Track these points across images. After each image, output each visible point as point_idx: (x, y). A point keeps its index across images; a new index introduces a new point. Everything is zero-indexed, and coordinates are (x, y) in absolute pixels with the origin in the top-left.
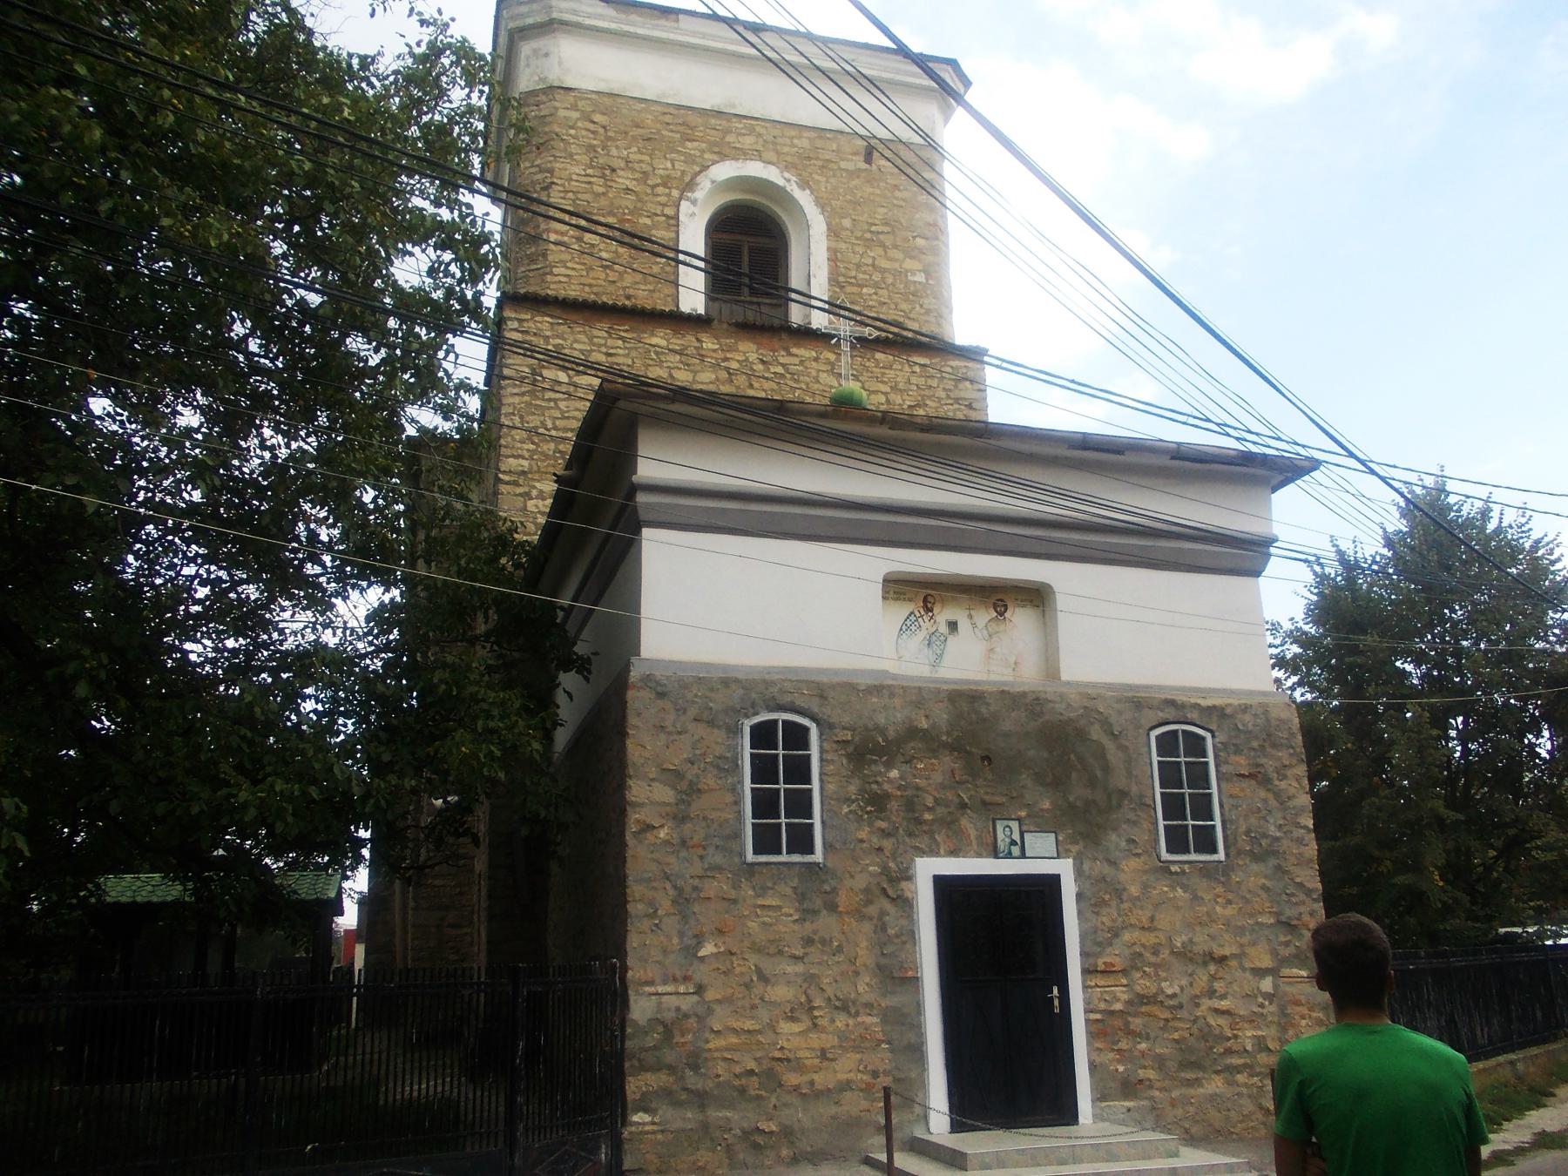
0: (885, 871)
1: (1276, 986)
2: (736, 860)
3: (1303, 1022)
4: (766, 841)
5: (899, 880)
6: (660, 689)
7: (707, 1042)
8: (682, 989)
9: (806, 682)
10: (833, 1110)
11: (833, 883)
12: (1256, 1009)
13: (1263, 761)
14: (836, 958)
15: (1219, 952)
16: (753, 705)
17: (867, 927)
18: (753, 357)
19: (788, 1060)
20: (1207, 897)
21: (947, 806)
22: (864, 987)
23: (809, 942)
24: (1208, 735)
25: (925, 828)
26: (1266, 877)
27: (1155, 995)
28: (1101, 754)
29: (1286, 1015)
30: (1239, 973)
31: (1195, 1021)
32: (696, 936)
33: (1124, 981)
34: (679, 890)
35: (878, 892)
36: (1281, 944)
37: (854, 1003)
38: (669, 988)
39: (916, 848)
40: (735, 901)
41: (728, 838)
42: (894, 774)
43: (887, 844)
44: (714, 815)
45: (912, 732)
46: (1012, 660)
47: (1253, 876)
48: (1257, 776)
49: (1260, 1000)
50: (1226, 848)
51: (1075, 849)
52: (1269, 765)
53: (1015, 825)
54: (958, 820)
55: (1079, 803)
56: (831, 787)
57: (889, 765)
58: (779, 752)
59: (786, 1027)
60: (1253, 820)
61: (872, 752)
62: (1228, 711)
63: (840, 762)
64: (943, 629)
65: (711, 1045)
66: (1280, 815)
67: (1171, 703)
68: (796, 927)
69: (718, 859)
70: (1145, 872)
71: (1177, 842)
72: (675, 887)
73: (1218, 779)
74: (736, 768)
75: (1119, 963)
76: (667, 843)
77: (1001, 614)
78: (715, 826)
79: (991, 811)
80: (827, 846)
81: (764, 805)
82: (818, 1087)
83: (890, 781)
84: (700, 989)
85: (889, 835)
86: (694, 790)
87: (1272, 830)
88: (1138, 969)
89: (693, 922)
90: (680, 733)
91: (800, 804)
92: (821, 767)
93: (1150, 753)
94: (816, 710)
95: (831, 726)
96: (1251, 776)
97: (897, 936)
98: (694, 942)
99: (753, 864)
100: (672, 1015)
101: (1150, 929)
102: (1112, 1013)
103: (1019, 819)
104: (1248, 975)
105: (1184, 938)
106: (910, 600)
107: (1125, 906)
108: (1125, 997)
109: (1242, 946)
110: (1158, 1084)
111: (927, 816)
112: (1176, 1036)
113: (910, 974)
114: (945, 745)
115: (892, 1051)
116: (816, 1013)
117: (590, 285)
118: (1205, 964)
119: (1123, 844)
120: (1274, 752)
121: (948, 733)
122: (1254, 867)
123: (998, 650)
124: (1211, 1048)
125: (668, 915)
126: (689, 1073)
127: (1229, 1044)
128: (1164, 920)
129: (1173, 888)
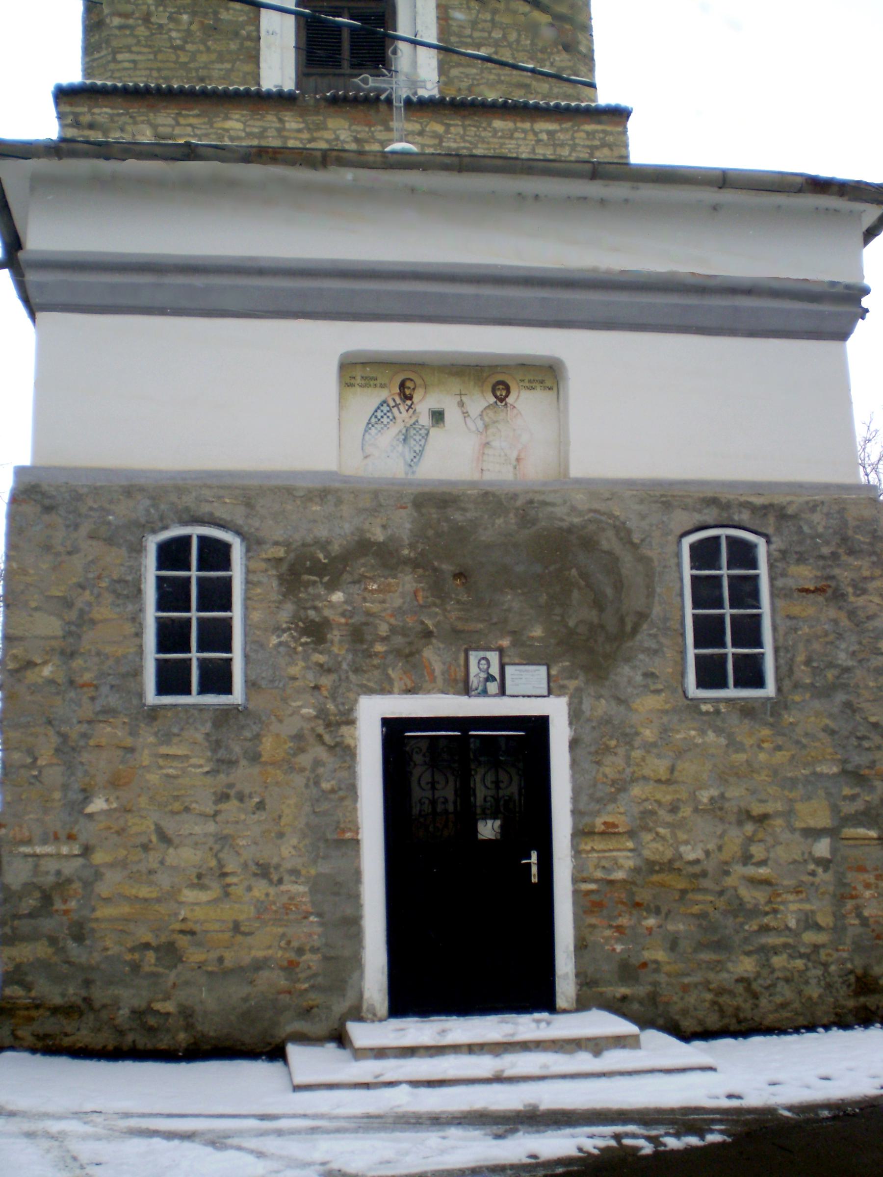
0: (322, 713)
1: (834, 850)
2: (135, 702)
3: (868, 894)
4: (172, 680)
5: (339, 724)
6: (47, 502)
7: (94, 910)
8: (65, 850)
9: (229, 487)
10: (246, 990)
11: (256, 728)
12: (807, 878)
13: (836, 571)
14: (256, 817)
15: (757, 809)
16: (162, 518)
17: (299, 780)
18: (344, 135)
19: (192, 933)
20: (748, 742)
21: (404, 635)
22: (288, 852)
23: (223, 797)
24: (761, 542)
25: (376, 661)
26: (831, 716)
27: (671, 861)
28: (612, 565)
29: (845, 885)
30: (786, 836)
31: (721, 893)
32: (84, 790)
33: (630, 844)
34: (64, 737)
35: (312, 740)
36: (845, 798)
37: (277, 867)
38: (49, 849)
39: (362, 686)
40: (132, 750)
41: (124, 676)
42: (337, 597)
43: (326, 681)
44: (108, 649)
45: (363, 546)
46: (514, 455)
47: (809, 716)
48: (827, 591)
49: (812, 867)
50: (779, 680)
51: (572, 684)
52: (844, 575)
53: (494, 657)
54: (419, 652)
55: (582, 629)
56: (256, 616)
57: (332, 587)
58: (193, 576)
59: (189, 895)
60: (816, 646)
61: (310, 571)
62: (790, 511)
63: (271, 585)
64: (425, 420)
65: (98, 914)
66: (854, 638)
67: (713, 501)
68: (209, 780)
69: (114, 700)
70: (665, 712)
71: (710, 674)
72: (59, 733)
73: (773, 595)
74: (138, 593)
75: (623, 823)
76: (51, 682)
77: (502, 400)
78: (111, 662)
79: (465, 640)
80: (251, 685)
81: (171, 637)
82: (228, 963)
83: (332, 605)
84: (87, 851)
85: (329, 671)
86: (85, 620)
87: (842, 658)
88: (650, 830)
89: (80, 774)
90: (69, 553)
91: (218, 636)
92: (246, 591)
93: (679, 565)
94: (240, 521)
95: (260, 542)
96: (818, 590)
97: (333, 791)
98: (81, 797)
99: (155, 709)
100: (51, 879)
101: (668, 782)
102: (611, 882)
103: (501, 651)
104: (797, 836)
105: (714, 792)
106: (382, 386)
107: (637, 754)
108: (630, 863)
109: (791, 801)
110: (667, 968)
111: (379, 648)
112: (696, 909)
113: (348, 835)
114: (407, 561)
115: (322, 924)
116: (229, 880)
117: (159, 70)
118: (740, 823)
119: (639, 678)
120: (850, 559)
121: (412, 546)
122: (817, 704)
123: (495, 444)
124: (742, 924)
125: (51, 765)
126: (71, 945)
127: (766, 920)
128: (688, 768)
129: (703, 732)
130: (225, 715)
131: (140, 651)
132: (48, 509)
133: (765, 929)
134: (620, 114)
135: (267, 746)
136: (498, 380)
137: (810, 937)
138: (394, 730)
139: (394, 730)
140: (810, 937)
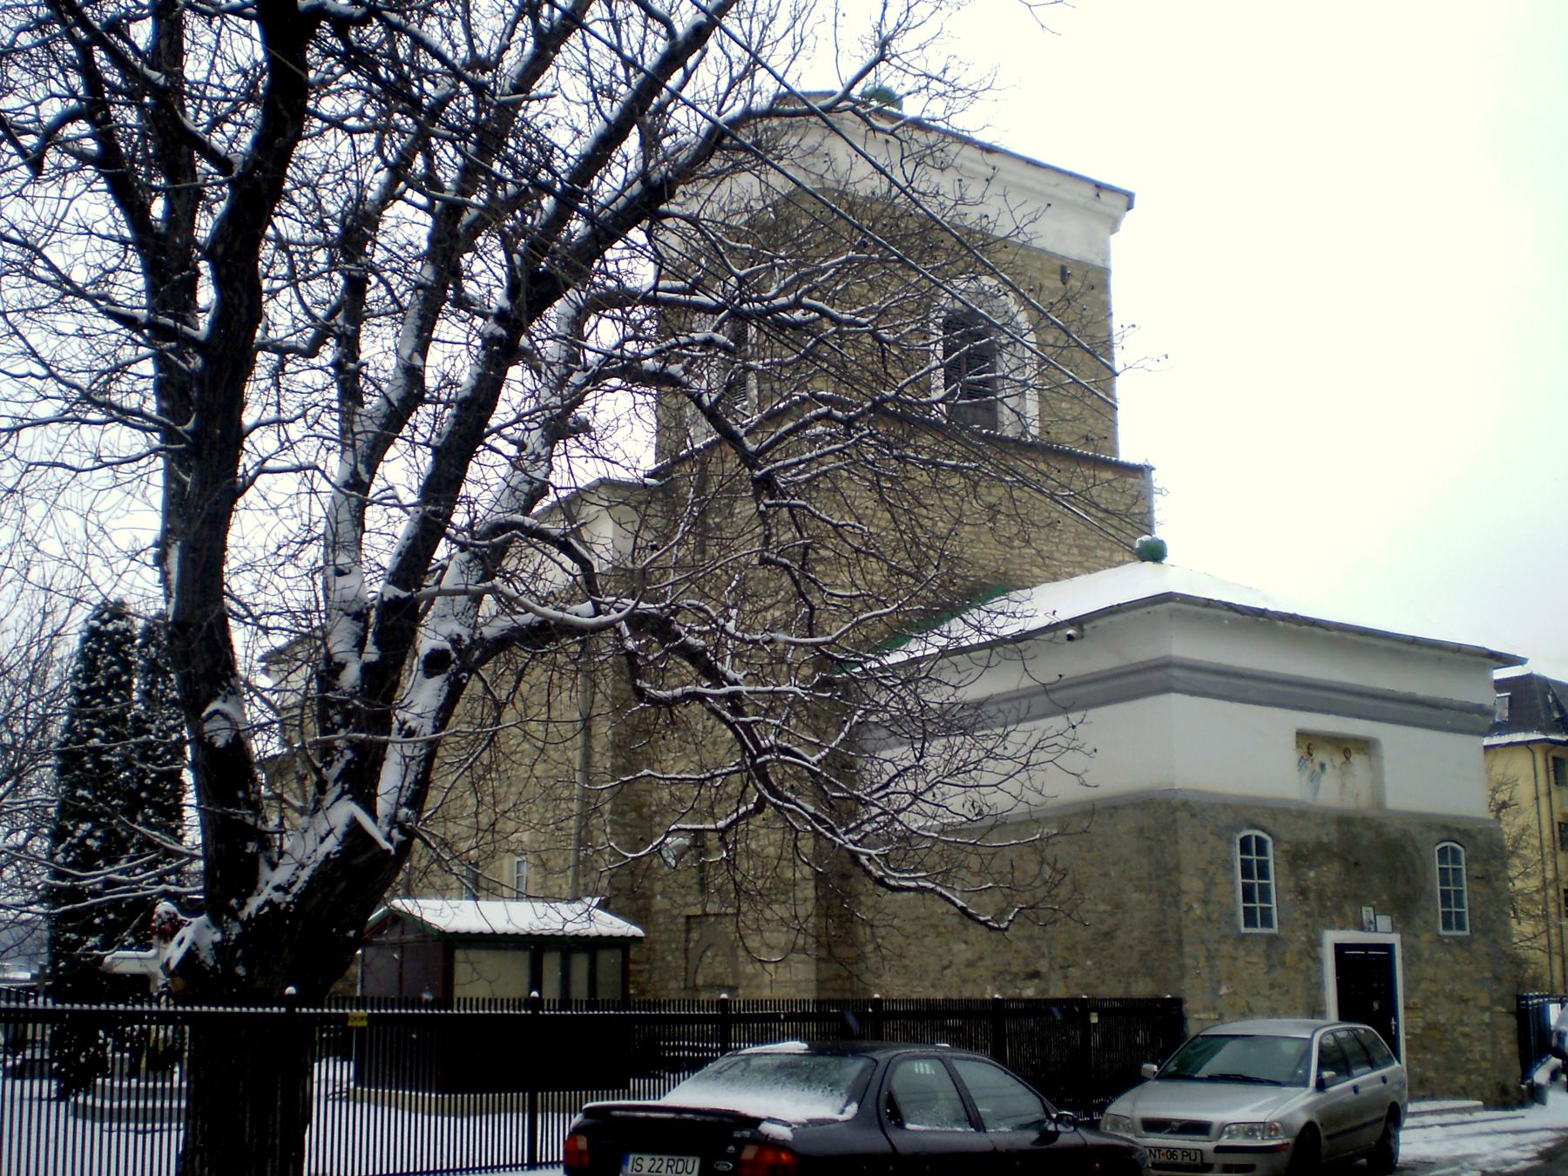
42: (1312, 874)
43: (1309, 921)
64: (1318, 769)
67: (1446, 827)
79: (1359, 901)
130: (1272, 940)
131: (1235, 902)
132: (1193, 815)
133: (1468, 1060)
134: (1141, 471)
135: (1288, 958)
136: (1346, 746)
137: (1484, 1065)
138: (1340, 948)
139: (1340, 948)
140: (1484, 1065)
